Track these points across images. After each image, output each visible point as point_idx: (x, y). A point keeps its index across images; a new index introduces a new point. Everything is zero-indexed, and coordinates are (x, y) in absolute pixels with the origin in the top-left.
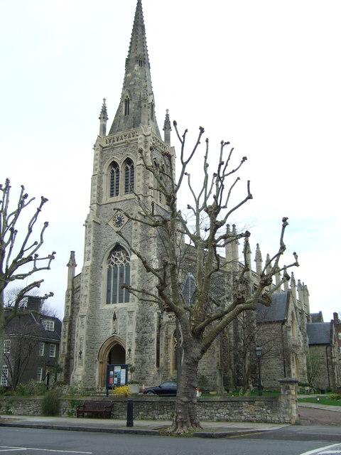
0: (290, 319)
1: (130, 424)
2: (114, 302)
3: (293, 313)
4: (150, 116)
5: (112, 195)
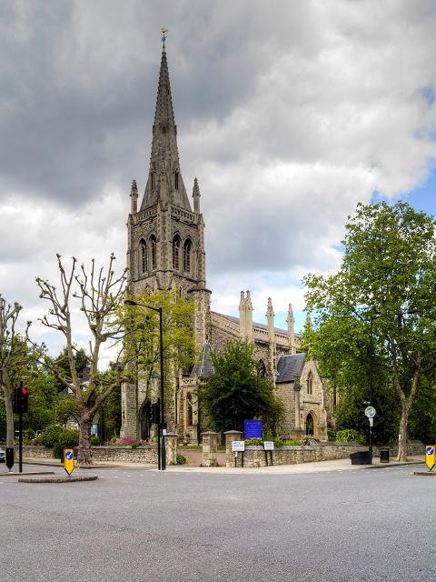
0: (303, 378)
3: (310, 373)
4: (173, 184)
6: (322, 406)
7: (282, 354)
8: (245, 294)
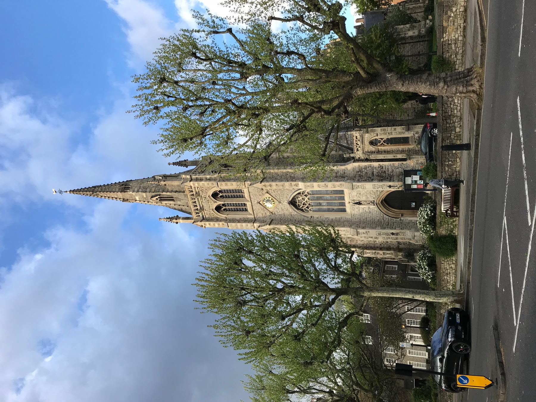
1: (467, 147)
2: (344, 204)
5: (246, 210)
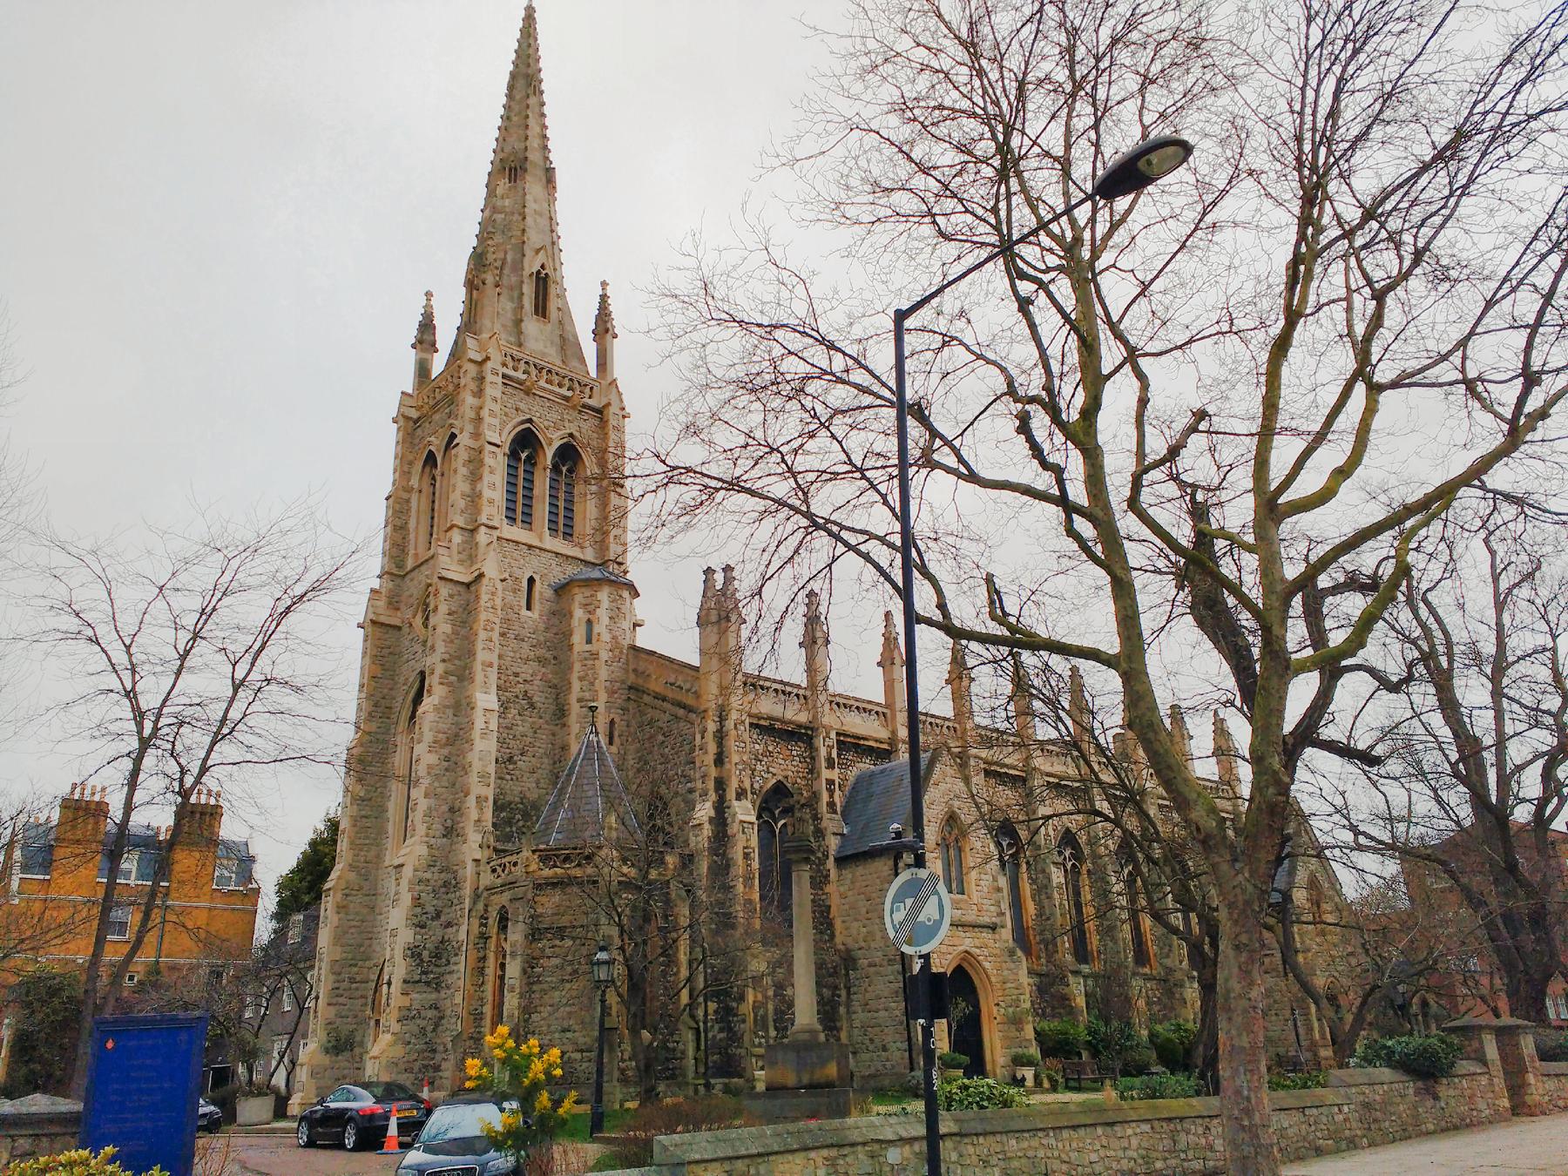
6: (1006, 934)
7: (865, 766)
8: (719, 578)
